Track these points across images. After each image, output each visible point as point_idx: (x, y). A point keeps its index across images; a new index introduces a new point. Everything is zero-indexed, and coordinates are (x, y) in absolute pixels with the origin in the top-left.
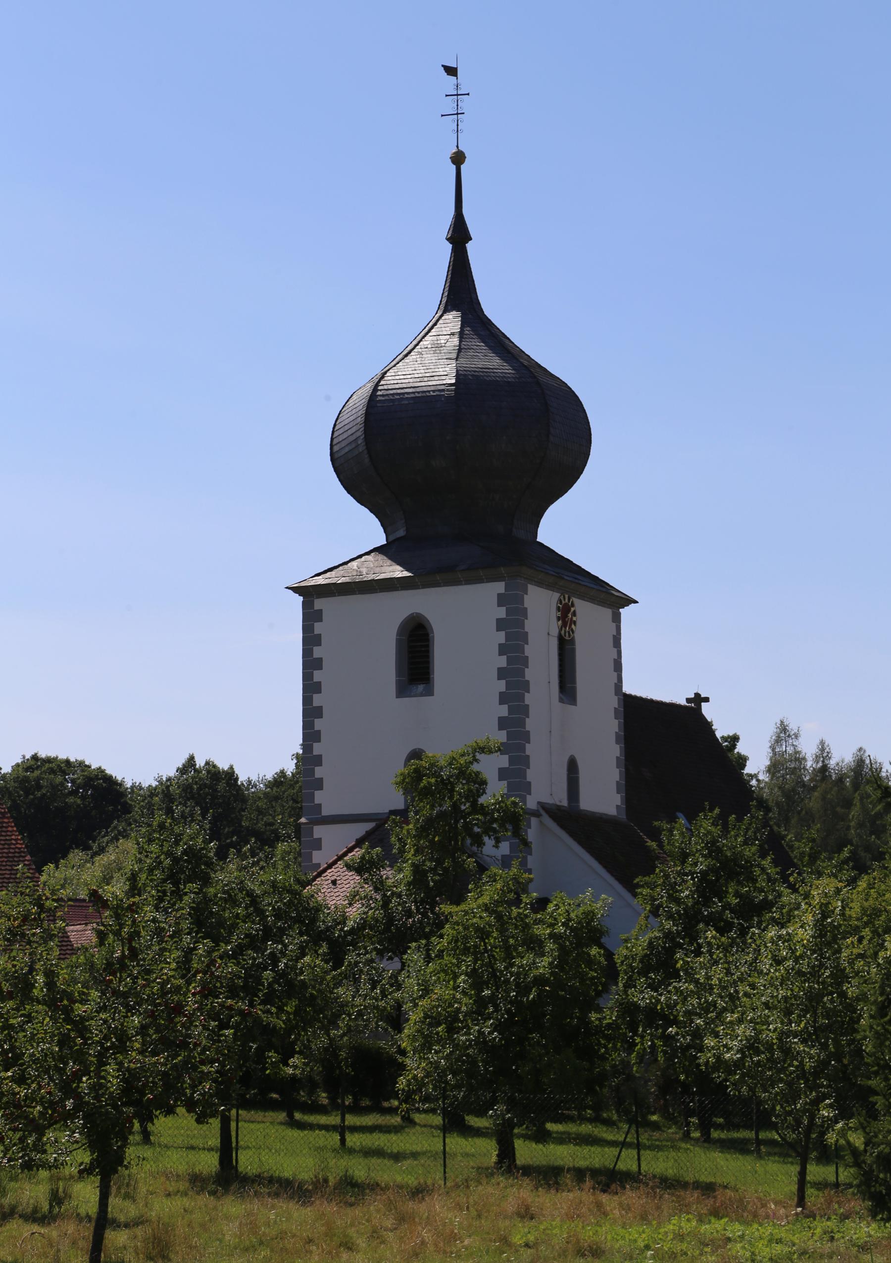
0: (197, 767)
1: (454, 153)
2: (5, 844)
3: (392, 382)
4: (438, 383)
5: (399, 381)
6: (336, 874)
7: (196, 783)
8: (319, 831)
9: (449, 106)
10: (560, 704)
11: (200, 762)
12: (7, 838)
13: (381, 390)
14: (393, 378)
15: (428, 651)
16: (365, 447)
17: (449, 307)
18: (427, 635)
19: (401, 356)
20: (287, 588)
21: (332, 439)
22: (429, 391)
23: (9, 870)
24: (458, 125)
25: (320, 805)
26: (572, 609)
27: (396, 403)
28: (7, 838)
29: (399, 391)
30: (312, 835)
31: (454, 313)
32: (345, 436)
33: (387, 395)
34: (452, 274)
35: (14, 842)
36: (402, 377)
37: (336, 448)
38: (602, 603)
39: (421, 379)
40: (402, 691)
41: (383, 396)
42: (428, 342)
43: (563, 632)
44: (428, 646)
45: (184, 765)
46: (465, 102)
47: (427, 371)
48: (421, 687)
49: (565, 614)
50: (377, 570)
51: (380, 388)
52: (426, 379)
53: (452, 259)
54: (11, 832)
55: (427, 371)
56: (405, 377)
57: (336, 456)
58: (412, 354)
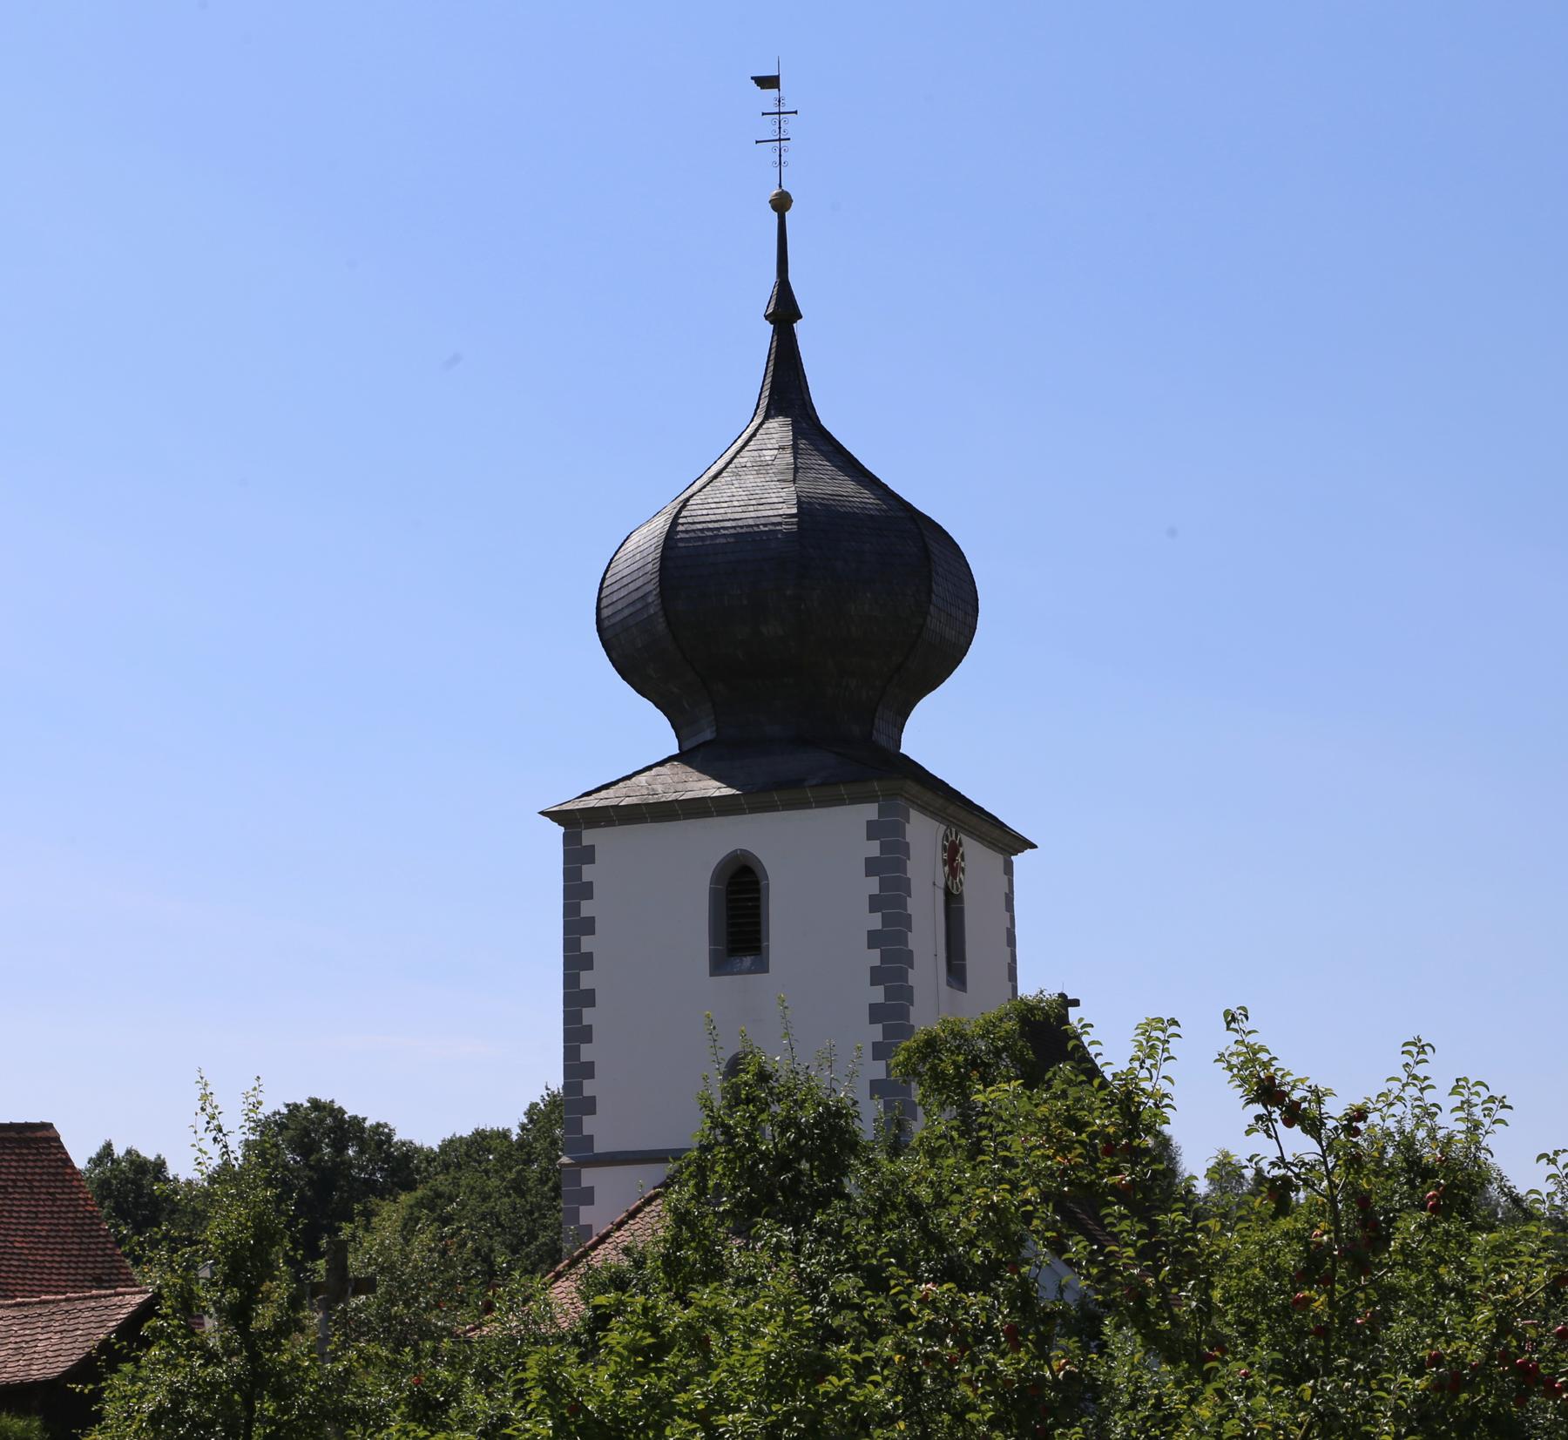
0: (115, 1157)
1: (776, 195)
2: (70, 1205)
3: (700, 512)
4: (771, 513)
5: (710, 512)
6: (628, 1239)
7: (116, 1177)
8: (589, 1177)
9: (768, 128)
10: (948, 988)
11: (119, 1151)
12: (73, 1196)
13: (682, 524)
14: (701, 507)
15: (758, 907)
16: (659, 607)
17: (773, 412)
18: (757, 883)
19: (705, 479)
20: (542, 813)
21: (599, 600)
22: (758, 525)
23: (77, 1243)
24: (780, 156)
25: (591, 1138)
26: (961, 850)
27: (708, 542)
28: (73, 1196)
29: (711, 526)
30: (579, 1183)
31: (781, 419)
32: (623, 593)
33: (693, 531)
34: (775, 365)
35: (82, 1202)
36: (713, 506)
37: (605, 613)
38: (992, 844)
39: (744, 509)
40: (719, 965)
41: (686, 532)
42: (745, 460)
43: (950, 883)
44: (758, 899)
45: (98, 1154)
46: (790, 124)
47: (751, 497)
48: (748, 961)
49: (952, 854)
50: (680, 787)
51: (681, 521)
52: (751, 508)
53: (775, 344)
54: (77, 1187)
55: (751, 497)
56: (718, 505)
57: (606, 624)
58: (724, 474)
